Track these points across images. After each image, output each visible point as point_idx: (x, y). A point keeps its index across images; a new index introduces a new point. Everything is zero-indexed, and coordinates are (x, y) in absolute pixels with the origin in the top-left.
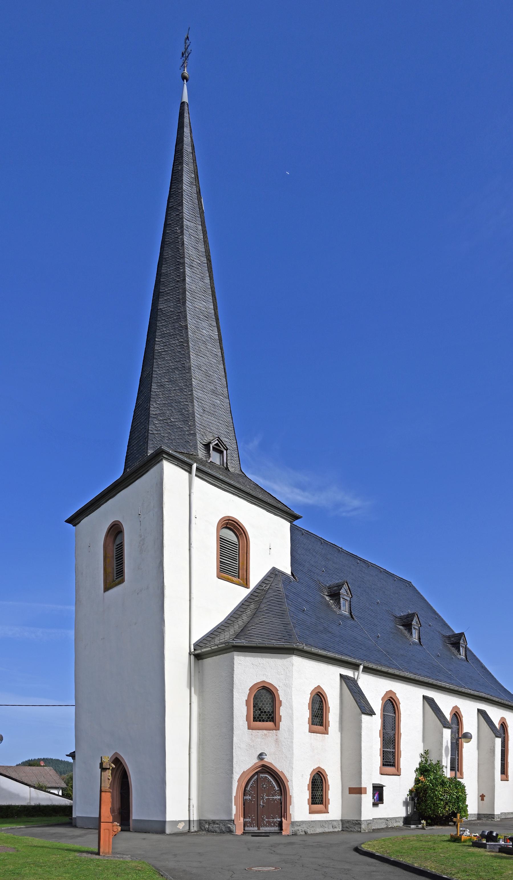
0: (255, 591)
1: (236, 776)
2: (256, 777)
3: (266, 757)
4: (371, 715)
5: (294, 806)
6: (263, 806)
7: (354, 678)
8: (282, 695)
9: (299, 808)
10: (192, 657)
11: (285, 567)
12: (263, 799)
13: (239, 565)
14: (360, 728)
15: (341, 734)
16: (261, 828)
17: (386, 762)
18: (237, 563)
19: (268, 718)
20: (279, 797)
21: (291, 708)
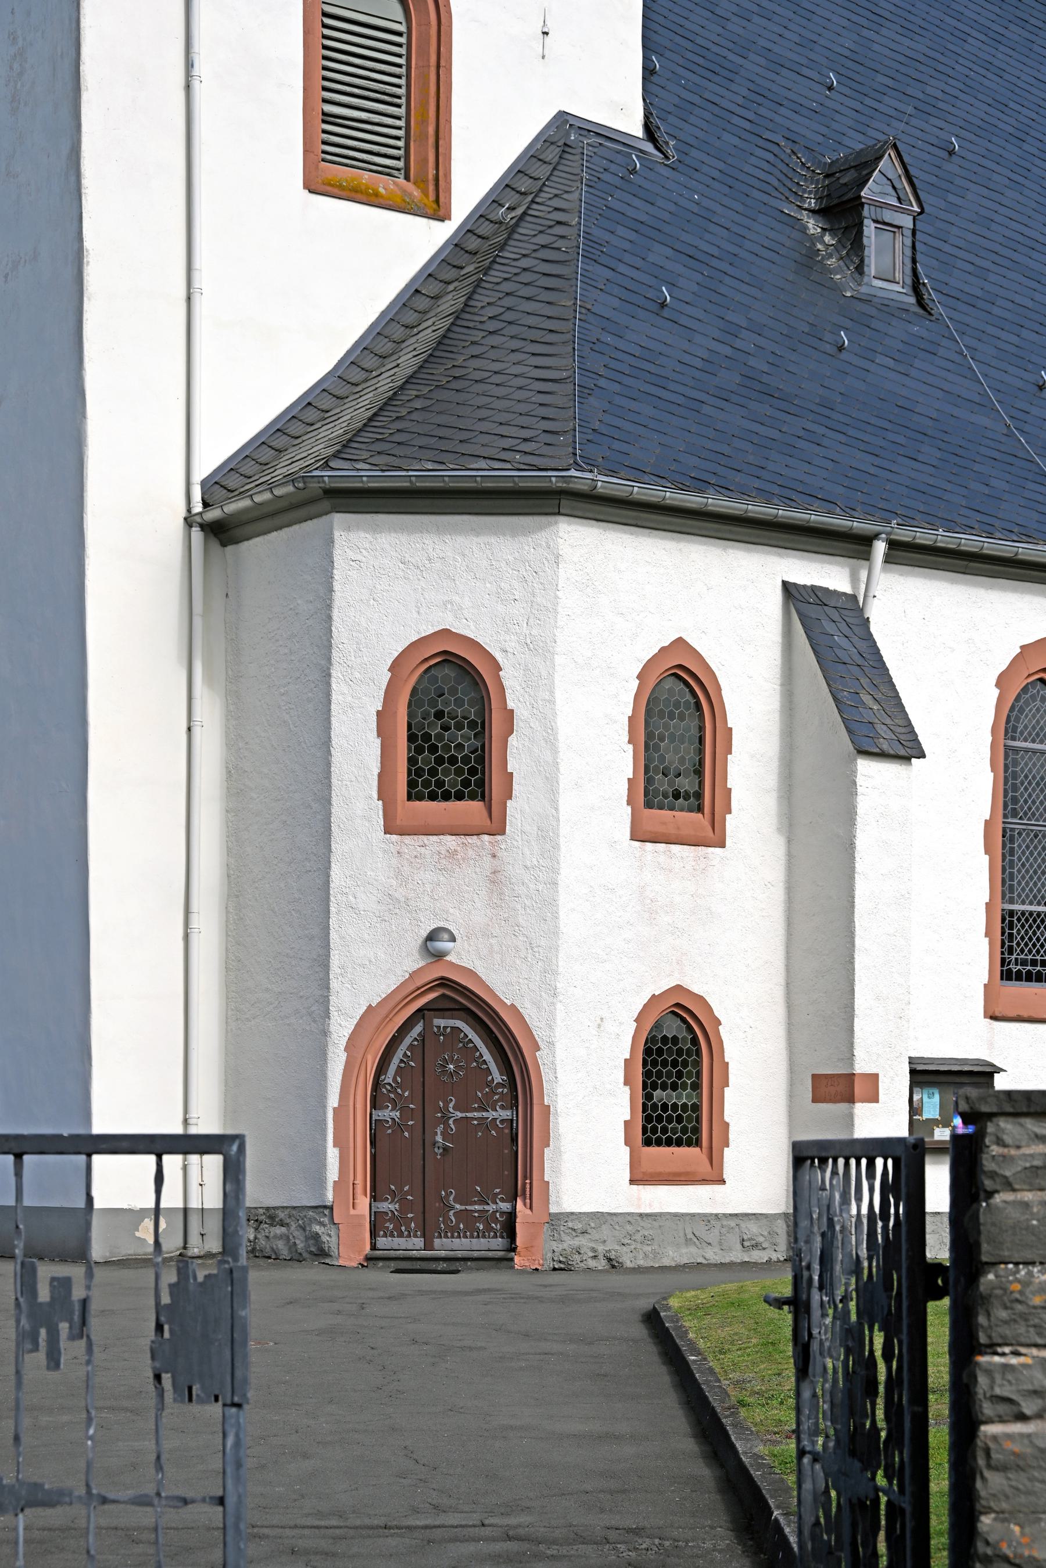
0: (468, 230)
1: (341, 1028)
2: (418, 1028)
3: (451, 945)
4: (906, 759)
5: (559, 1152)
6: (446, 1149)
7: (854, 598)
8: (516, 690)
9: (586, 1156)
10: (197, 534)
11: (615, 100)
12: (445, 1119)
13: (408, 122)
14: (849, 816)
15: (789, 842)
16: (437, 1242)
17: (1024, 963)
18: (401, 112)
19: (466, 783)
20: (506, 1114)
21: (551, 742)
